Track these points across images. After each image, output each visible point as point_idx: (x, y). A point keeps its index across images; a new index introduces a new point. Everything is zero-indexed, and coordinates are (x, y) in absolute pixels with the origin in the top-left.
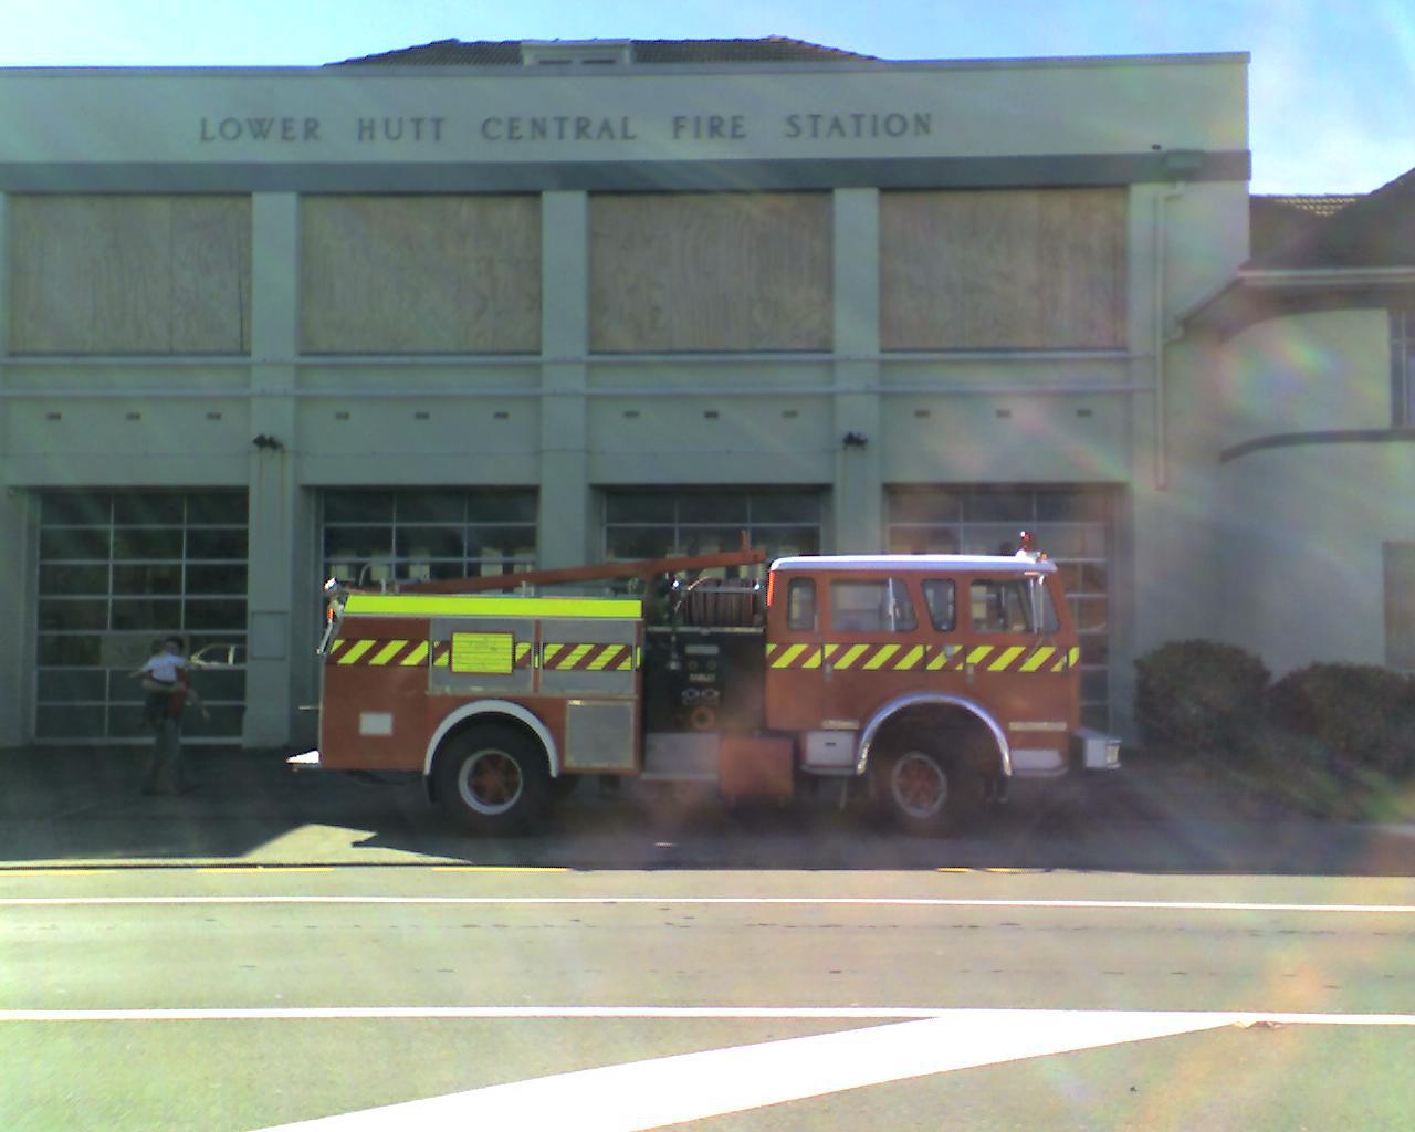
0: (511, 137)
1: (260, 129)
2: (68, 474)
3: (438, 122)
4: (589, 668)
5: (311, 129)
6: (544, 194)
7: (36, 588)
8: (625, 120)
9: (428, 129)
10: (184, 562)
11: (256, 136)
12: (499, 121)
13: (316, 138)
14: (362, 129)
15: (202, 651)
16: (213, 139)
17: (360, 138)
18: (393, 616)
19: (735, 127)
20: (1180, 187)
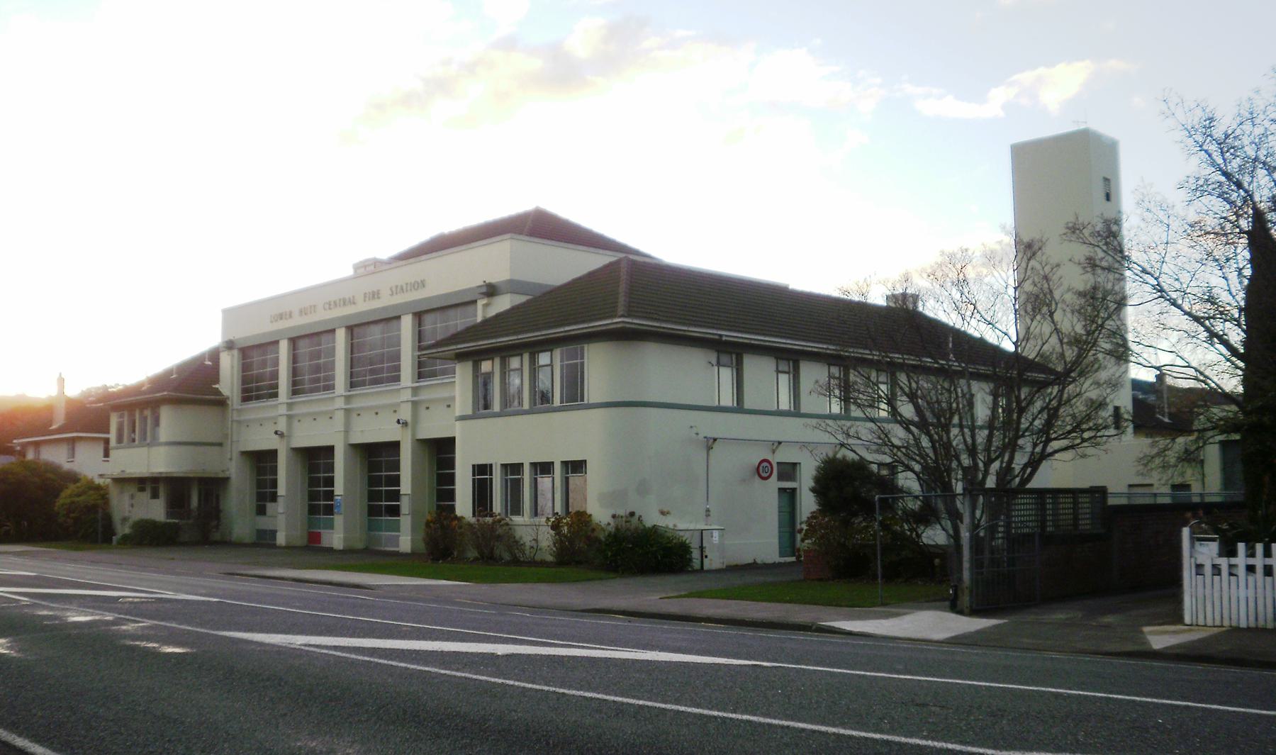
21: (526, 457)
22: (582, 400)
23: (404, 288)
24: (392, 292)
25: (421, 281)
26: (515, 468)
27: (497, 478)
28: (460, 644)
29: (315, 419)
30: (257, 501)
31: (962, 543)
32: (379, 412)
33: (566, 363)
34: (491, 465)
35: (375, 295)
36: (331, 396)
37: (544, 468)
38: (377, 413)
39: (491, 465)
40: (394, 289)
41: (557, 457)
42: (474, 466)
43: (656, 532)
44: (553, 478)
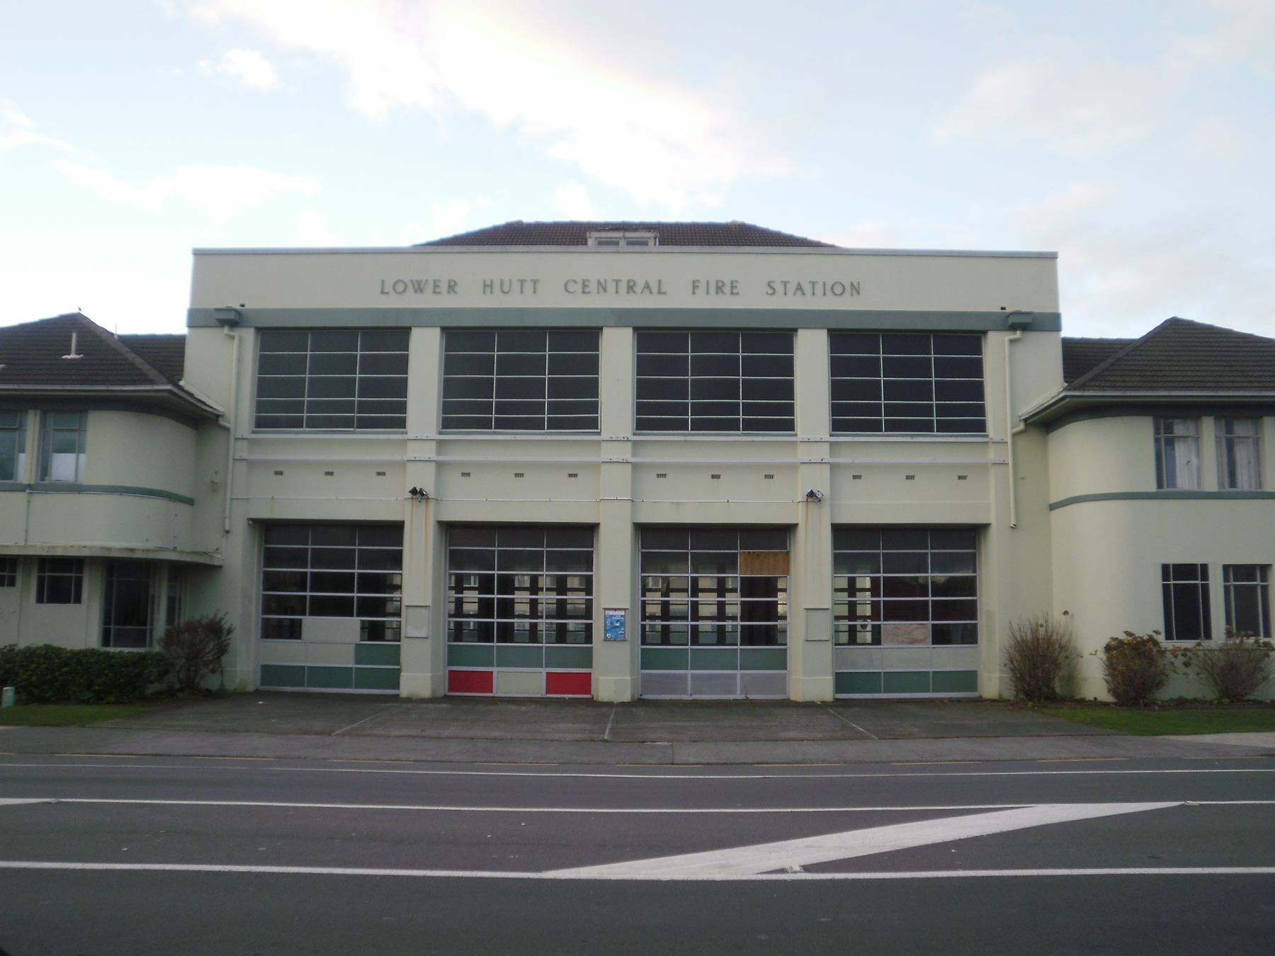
3: (535, 282)
11: (416, 292)
14: (485, 286)
20: (1018, 334)
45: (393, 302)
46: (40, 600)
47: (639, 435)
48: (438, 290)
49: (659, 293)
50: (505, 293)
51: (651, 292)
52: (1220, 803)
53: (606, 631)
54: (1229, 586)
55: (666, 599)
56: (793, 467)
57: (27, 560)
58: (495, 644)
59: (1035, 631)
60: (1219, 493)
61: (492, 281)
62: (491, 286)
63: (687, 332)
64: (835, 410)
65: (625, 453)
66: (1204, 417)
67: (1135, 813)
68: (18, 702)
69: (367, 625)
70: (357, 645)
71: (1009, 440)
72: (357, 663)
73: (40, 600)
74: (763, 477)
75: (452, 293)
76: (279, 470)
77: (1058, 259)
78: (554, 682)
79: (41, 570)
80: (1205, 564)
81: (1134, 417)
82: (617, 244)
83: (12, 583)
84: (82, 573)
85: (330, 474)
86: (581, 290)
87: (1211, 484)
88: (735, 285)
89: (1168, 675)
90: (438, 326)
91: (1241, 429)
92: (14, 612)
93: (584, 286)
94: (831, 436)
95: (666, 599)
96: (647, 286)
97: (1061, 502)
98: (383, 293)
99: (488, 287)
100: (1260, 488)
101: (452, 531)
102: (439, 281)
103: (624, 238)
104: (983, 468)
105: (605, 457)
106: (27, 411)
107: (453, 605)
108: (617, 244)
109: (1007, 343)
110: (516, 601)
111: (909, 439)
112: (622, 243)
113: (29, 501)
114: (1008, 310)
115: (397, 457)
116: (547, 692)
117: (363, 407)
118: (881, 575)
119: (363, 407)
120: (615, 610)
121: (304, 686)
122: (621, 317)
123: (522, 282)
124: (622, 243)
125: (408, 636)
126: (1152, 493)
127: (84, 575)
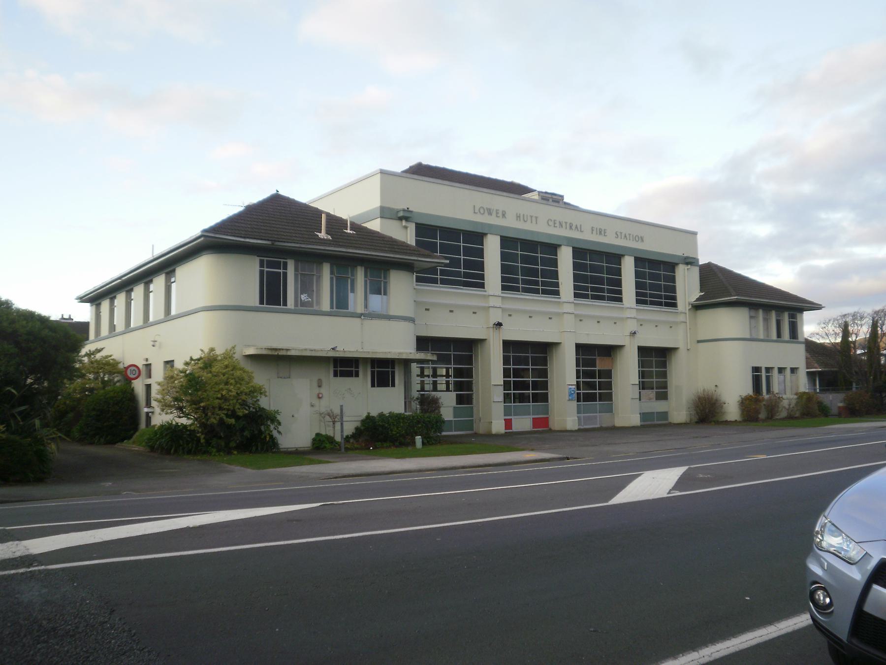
0: (554, 226)
1: (490, 212)
2: (503, 414)
3: (536, 218)
4: (774, 418)
5: (504, 215)
6: (563, 246)
7: (474, 397)
8: (418, 391)
9: (534, 219)
10: (655, 380)
11: (489, 214)
12: (551, 220)
13: (505, 217)
14: (517, 217)
15: (346, 231)
16: (477, 213)
17: (517, 220)
18: (237, 253)
19: (605, 233)
20: (689, 266)
21: (776, 365)
22: (285, 304)
23: (628, 236)
24: (617, 235)
25: (605, 230)
26: (768, 370)
27: (764, 374)
28: (145, 558)
29: (615, 323)
30: (667, 391)
31: (365, 418)
32: (617, 324)
33: (281, 271)
34: (761, 367)
35: (601, 232)
36: (556, 300)
37: (781, 370)
38: (656, 326)
39: (761, 367)
40: (619, 234)
41: (789, 366)
42: (753, 367)
43: (715, 404)
44: (785, 376)
45: (479, 218)
46: (373, 385)
47: (638, 306)
48: (556, 225)
49: (581, 231)
50: (483, 214)
51: (627, 239)
52: (28, 526)
53: (569, 396)
54: (580, 370)
55: (422, 379)
56: (622, 319)
57: (365, 360)
58: (598, 403)
59: (704, 390)
60: (750, 339)
61: (520, 214)
62: (519, 217)
63: (436, 228)
64: (503, 279)
65: (633, 314)
66: (391, 270)
67: (264, 507)
68: (423, 443)
69: (518, 396)
70: (454, 408)
71: (687, 312)
72: (454, 418)
73: (373, 385)
74: (424, 309)
75: (504, 218)
76: (581, 319)
77: (698, 235)
78: (536, 422)
79: (373, 367)
80: (758, 367)
81: (228, 254)
82: (548, 200)
83: (357, 375)
84: (358, 368)
85: (451, 311)
86: (553, 225)
87: (762, 337)
88: (606, 231)
89: (697, 407)
90: (498, 235)
91: (773, 315)
92: (360, 393)
93: (555, 223)
94: (502, 293)
95: (422, 379)
96: (576, 227)
97: (704, 340)
98: (475, 213)
99: (518, 217)
100: (768, 337)
101: (508, 345)
102: (499, 210)
103: (552, 198)
104: (676, 323)
105: (491, 304)
106: (356, 266)
107: (419, 385)
108: (548, 200)
109: (686, 270)
110: (425, 383)
111: (659, 309)
112: (551, 200)
113: (362, 324)
114: (685, 255)
115: (482, 303)
116: (533, 428)
117: (466, 275)
118: (581, 368)
119: (466, 275)
120: (572, 385)
121: (452, 431)
122: (569, 241)
123: (531, 217)
124: (551, 200)
125: (638, 397)
126: (748, 338)
127: (359, 369)
